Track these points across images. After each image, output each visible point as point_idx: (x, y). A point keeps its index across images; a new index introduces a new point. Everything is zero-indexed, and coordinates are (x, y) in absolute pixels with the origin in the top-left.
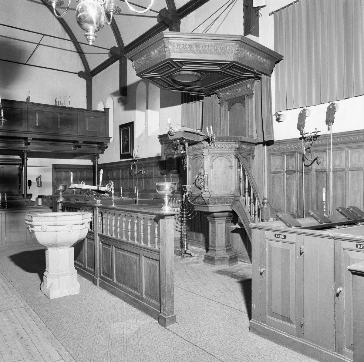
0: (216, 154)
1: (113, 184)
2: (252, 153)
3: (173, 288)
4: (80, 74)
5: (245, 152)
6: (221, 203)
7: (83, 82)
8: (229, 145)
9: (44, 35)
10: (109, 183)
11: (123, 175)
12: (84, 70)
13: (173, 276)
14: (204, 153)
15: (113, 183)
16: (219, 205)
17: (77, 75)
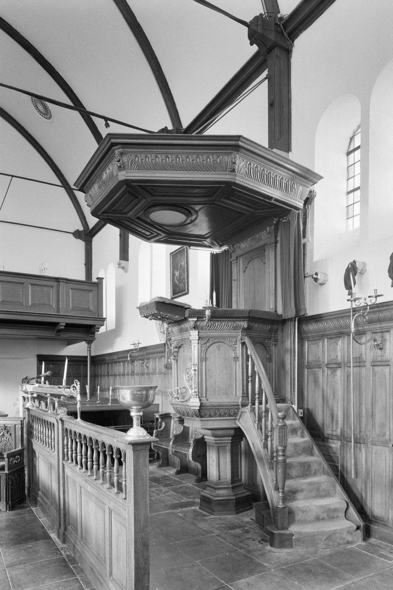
0: (212, 337)
1: (79, 386)
2: (273, 335)
3: (147, 575)
4: (77, 234)
5: (261, 334)
6: (220, 416)
7: (81, 244)
8: (232, 323)
9: (13, 176)
10: (74, 384)
11: (124, 371)
12: (81, 228)
13: (148, 552)
14: (192, 336)
15: (79, 383)
16: (217, 418)
17: (72, 235)
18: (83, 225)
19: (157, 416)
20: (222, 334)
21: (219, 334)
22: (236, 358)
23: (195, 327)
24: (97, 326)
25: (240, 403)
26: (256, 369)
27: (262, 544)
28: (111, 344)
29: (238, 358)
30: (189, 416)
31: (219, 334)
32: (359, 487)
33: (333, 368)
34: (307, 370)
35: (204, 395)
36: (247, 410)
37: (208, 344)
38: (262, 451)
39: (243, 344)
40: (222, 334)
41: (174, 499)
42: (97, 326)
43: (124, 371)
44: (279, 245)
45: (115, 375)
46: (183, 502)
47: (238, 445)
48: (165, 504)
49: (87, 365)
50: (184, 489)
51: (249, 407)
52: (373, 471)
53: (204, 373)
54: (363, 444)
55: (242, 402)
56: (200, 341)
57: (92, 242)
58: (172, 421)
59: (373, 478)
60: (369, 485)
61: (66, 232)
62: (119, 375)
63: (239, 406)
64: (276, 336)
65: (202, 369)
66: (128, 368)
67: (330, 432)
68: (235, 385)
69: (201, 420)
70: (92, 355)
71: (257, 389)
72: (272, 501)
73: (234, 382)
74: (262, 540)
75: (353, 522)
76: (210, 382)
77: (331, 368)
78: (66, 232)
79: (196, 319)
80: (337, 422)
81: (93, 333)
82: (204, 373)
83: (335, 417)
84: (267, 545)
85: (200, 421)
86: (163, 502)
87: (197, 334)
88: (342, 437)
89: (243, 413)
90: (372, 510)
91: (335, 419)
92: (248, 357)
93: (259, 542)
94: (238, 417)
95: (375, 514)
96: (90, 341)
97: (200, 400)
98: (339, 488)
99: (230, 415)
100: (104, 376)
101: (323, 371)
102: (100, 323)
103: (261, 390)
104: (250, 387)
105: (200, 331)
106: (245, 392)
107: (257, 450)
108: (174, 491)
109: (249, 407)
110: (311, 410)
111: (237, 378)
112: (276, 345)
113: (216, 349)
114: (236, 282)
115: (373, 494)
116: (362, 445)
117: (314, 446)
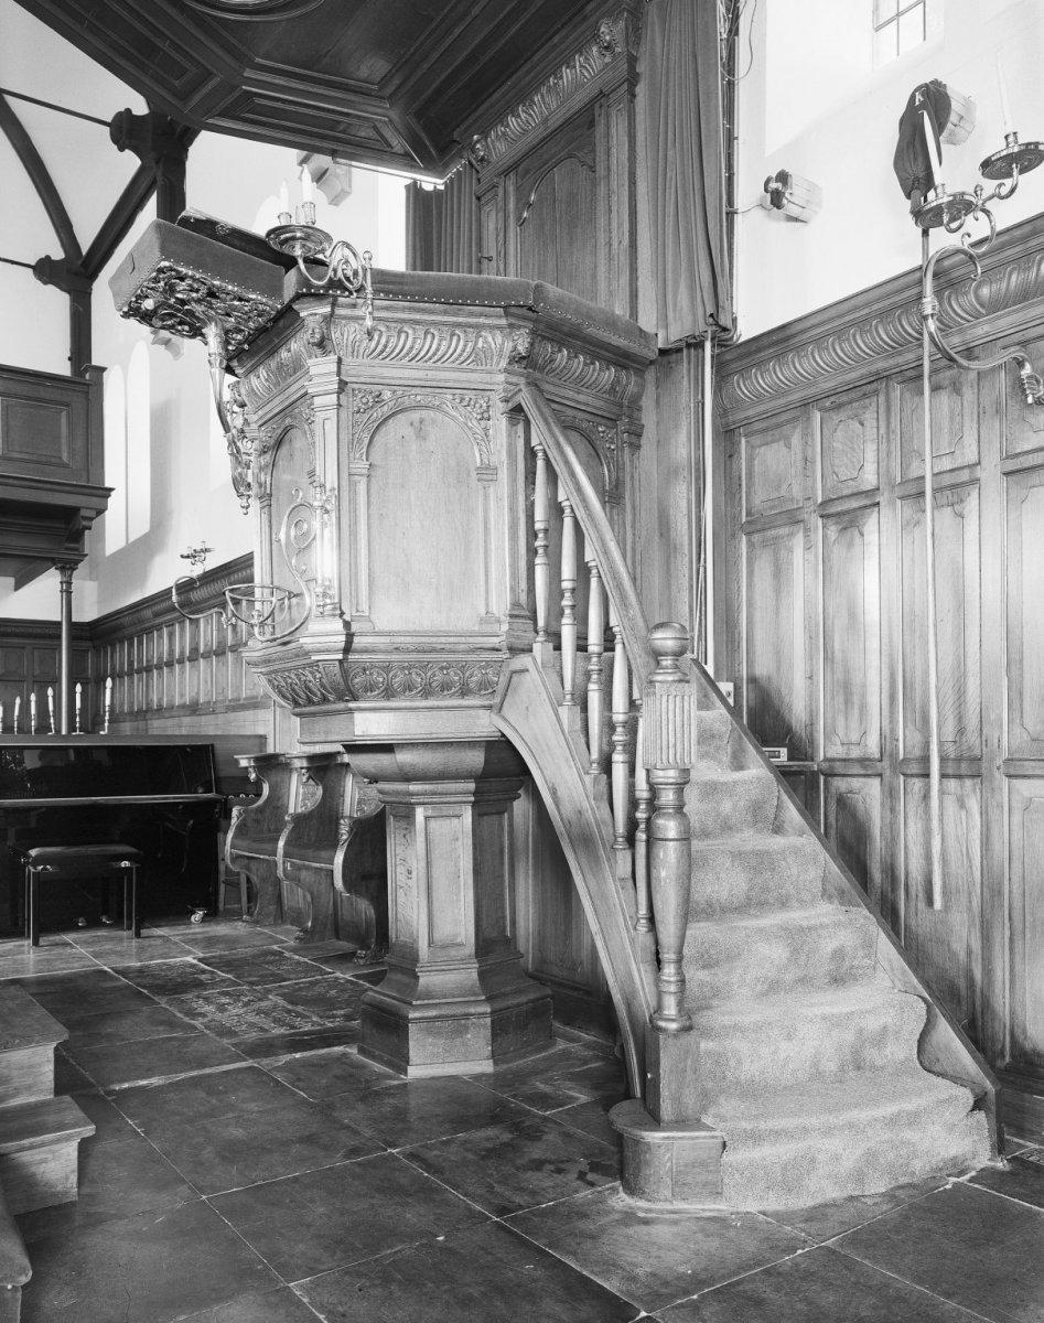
4: (45, 270)
6: (427, 692)
7: (57, 301)
11: (171, 651)
12: (58, 254)
17: (30, 271)
18: (63, 245)
19: (244, 763)
22: (487, 472)
24: (84, 513)
27: (592, 1184)
28: (141, 577)
30: (314, 704)
32: (959, 948)
33: (847, 512)
34: (749, 541)
36: (531, 667)
38: (594, 812)
39: (517, 412)
41: (275, 1021)
42: (84, 513)
43: (171, 651)
44: (641, 89)
45: (148, 670)
46: (306, 1033)
47: (501, 813)
48: (235, 1040)
50: (318, 989)
52: (1015, 879)
54: (973, 776)
57: (90, 294)
58: (295, 777)
59: (1017, 904)
60: (1001, 937)
61: (13, 262)
62: (159, 667)
66: (182, 639)
67: (837, 751)
72: (629, 1006)
74: (594, 1168)
75: (956, 1079)
77: (838, 514)
78: (13, 262)
80: (863, 708)
81: (77, 536)
83: (856, 690)
84: (614, 1190)
86: (230, 1033)
88: (886, 763)
89: (515, 678)
90: (1018, 1031)
91: (856, 699)
92: (531, 454)
93: (582, 1176)
95: (1028, 1046)
98: (885, 946)
101: (807, 530)
102: (94, 502)
106: (523, 598)
107: (567, 809)
108: (284, 996)
110: (763, 683)
113: (409, 432)
114: (494, 263)
115: (1018, 967)
116: (968, 782)
117: (785, 797)
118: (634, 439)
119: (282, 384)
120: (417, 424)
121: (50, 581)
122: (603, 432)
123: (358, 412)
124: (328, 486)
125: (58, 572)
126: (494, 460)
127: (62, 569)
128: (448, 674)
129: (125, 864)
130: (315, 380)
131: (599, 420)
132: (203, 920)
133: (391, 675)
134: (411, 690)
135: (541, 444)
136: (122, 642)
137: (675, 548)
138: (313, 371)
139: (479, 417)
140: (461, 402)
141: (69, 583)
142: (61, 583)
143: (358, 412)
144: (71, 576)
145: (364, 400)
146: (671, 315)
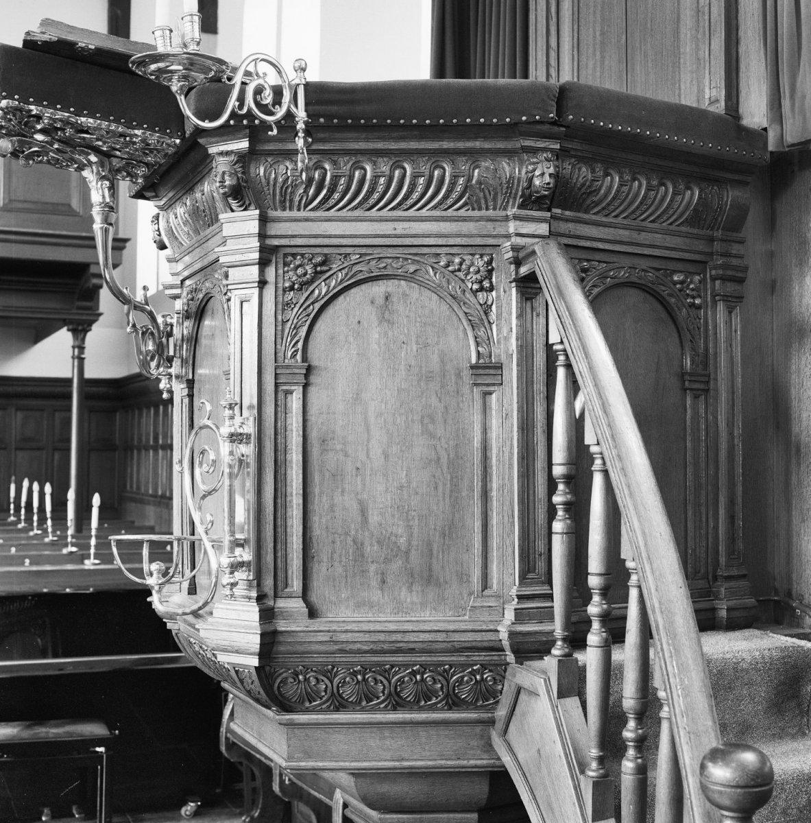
5: (644, 237)
16: (379, 717)
20: (401, 227)
21: (386, 228)
23: (240, 193)
25: (504, 635)
26: (589, 439)
29: (499, 367)
31: (386, 228)
35: (296, 585)
37: (322, 289)
40: (401, 227)
49: (69, 409)
51: (550, 663)
53: (295, 457)
55: (512, 635)
56: (271, 273)
63: (503, 650)
64: (735, 249)
65: (280, 432)
68: (478, 525)
69: (290, 725)
70: (88, 374)
71: (595, 562)
73: (477, 510)
76: (332, 508)
79: (244, 144)
82: (295, 457)
85: (284, 729)
87: (254, 227)
94: (501, 712)
96: (80, 322)
97: (267, 615)
99: (454, 702)
100: (147, 449)
103: (617, 575)
104: (559, 547)
105: (272, 213)
109: (550, 663)
111: (495, 485)
112: (733, 301)
113: (370, 315)
118: (730, 288)
119: (202, 234)
120: (380, 301)
121: (63, 338)
122: (682, 282)
123: (292, 288)
124: (246, 404)
125: (70, 335)
126: (498, 353)
127: (74, 331)
128: (423, 680)
129: (101, 749)
130: (231, 245)
131: (671, 266)
132: (197, 814)
133: (336, 680)
134: (369, 700)
135: (562, 342)
136: (148, 408)
137: (798, 450)
138: (228, 230)
139: (475, 287)
140: (448, 266)
141: (81, 348)
142: (74, 347)
143: (292, 288)
144: (83, 340)
145: (300, 271)
146: (786, 103)
